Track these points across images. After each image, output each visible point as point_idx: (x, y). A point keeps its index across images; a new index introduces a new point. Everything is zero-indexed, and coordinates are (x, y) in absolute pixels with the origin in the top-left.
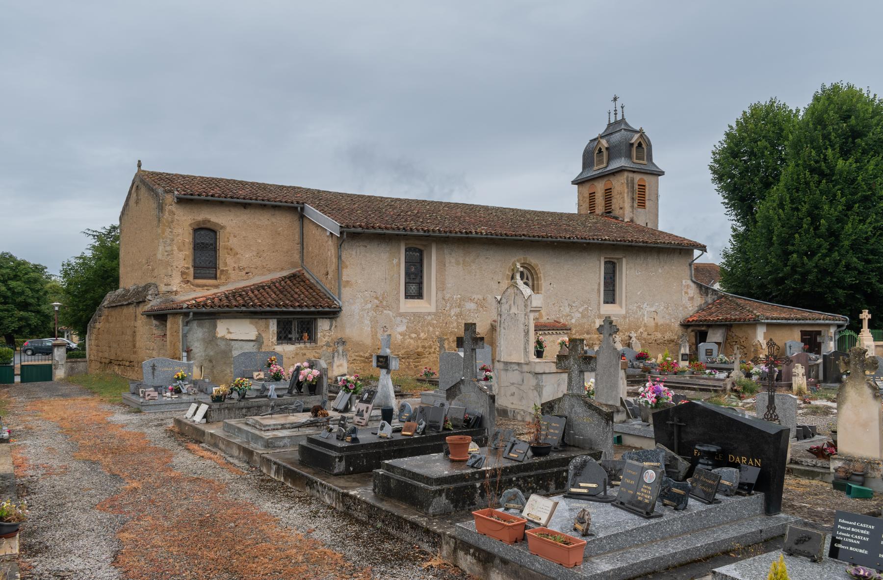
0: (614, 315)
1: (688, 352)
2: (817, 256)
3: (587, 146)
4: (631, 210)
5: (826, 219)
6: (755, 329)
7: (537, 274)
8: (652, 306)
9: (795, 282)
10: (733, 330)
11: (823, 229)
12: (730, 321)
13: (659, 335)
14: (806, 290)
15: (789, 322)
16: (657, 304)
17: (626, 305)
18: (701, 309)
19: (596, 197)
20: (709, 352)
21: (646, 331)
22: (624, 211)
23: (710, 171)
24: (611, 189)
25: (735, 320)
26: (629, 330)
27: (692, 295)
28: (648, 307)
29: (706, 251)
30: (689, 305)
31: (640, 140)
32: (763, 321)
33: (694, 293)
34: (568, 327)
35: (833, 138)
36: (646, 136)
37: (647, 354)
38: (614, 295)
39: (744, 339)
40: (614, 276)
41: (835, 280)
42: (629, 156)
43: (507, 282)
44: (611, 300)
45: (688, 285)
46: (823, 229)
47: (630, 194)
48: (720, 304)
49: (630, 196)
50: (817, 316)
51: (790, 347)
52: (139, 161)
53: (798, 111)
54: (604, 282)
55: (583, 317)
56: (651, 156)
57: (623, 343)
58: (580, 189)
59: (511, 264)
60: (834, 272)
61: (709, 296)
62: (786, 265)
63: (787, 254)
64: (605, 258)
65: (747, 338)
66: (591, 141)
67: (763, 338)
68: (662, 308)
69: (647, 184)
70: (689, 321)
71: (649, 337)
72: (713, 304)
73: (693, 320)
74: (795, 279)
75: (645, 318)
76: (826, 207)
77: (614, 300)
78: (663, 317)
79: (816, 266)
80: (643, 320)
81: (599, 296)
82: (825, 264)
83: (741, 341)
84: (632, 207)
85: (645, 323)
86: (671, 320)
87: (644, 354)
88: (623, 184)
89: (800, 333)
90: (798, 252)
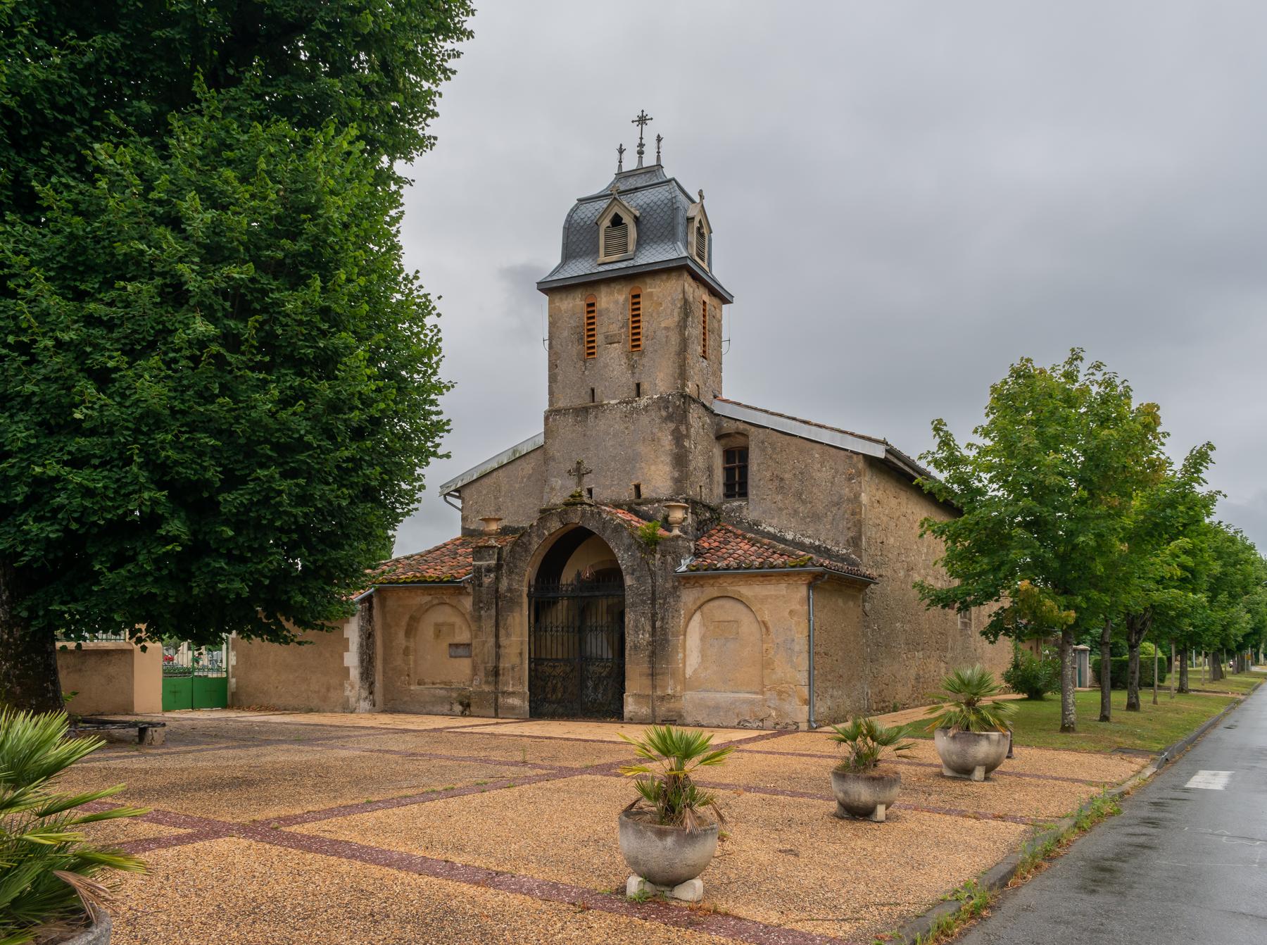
52: (659, 136)
53: (395, 530)
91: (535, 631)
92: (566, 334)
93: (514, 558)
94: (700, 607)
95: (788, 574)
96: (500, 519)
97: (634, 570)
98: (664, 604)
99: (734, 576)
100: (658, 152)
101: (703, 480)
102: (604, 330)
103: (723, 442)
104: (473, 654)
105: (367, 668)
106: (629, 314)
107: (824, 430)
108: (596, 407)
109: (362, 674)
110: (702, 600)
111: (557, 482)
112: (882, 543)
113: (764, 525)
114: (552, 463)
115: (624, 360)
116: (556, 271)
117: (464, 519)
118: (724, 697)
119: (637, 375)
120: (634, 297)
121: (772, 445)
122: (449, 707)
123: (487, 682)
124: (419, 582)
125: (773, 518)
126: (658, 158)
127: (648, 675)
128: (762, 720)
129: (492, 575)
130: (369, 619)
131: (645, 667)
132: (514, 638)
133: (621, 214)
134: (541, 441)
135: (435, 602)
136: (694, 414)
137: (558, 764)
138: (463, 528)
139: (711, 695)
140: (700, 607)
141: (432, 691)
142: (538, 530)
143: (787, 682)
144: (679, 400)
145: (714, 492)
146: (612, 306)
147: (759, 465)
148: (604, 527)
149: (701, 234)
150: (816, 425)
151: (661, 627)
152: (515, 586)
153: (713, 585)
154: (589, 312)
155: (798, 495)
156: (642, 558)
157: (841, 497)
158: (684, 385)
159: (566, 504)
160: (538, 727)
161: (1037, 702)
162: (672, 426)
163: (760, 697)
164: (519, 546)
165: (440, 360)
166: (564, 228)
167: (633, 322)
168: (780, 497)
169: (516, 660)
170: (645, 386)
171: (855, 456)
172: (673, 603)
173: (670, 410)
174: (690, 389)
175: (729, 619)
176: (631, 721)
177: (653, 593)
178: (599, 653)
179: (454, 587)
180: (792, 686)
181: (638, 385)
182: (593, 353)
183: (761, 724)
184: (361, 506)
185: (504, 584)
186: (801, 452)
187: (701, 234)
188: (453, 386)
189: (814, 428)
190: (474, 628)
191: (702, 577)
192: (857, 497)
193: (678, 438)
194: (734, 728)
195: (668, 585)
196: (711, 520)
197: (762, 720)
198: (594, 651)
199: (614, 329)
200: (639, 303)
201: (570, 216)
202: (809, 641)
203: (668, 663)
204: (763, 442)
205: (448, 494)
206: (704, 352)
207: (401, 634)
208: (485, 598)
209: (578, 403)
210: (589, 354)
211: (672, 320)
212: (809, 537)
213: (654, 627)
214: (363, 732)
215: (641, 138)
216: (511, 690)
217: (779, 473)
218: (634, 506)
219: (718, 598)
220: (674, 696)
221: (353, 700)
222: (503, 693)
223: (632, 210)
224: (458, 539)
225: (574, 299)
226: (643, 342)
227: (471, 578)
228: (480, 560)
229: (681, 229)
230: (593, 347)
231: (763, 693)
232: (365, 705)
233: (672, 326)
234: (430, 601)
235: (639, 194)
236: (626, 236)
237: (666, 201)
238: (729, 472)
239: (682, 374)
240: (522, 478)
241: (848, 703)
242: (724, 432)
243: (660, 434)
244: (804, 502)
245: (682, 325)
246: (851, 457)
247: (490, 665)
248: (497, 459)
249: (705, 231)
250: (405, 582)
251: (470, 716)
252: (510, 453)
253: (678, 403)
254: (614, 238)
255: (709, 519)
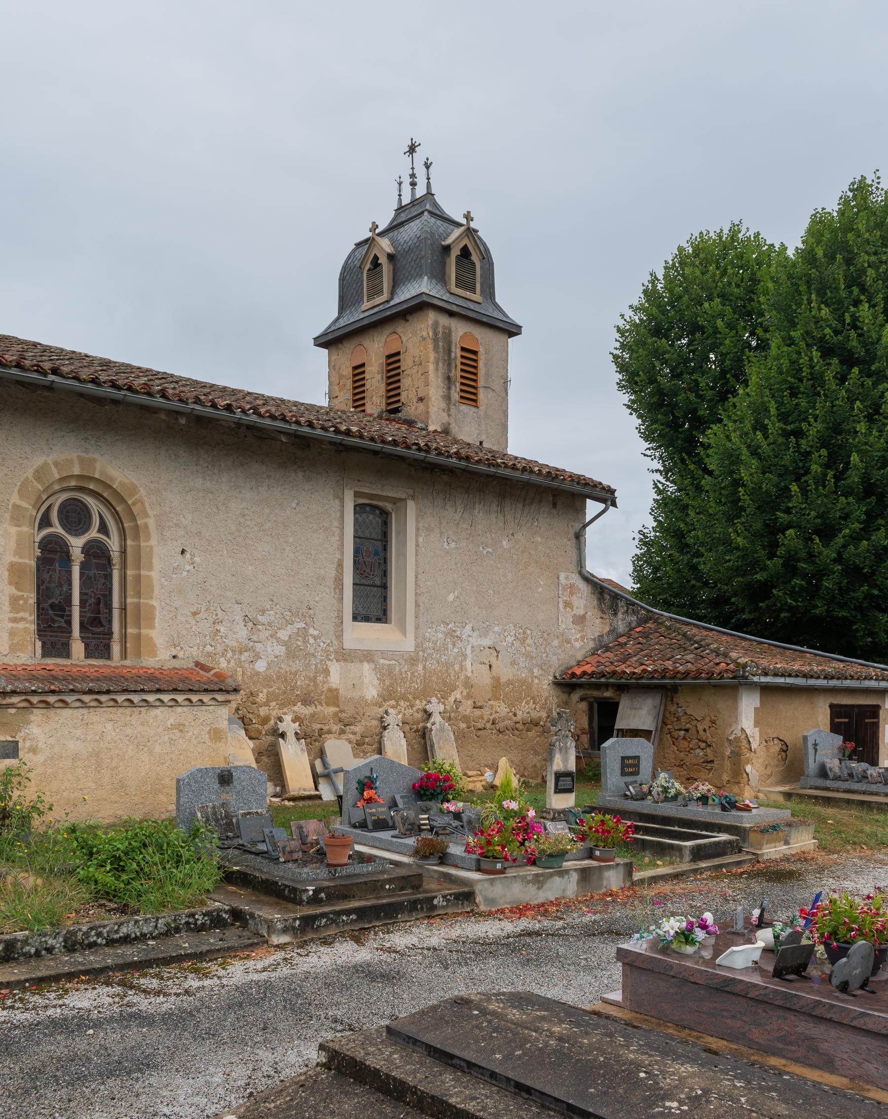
0: (382, 652)
1: (572, 766)
2: (840, 535)
3: (349, 257)
4: (443, 405)
5: (862, 453)
6: (735, 699)
7: (133, 518)
8: (484, 634)
9: (793, 594)
10: (680, 699)
11: (854, 478)
12: (674, 678)
13: (503, 709)
14: (817, 611)
15: (811, 682)
16: (496, 629)
17: (417, 628)
18: (602, 646)
19: (367, 376)
20: (631, 766)
21: (469, 696)
22: (427, 407)
23: (614, 367)
24: (398, 353)
25: (687, 674)
26: (425, 693)
27: (581, 612)
28: (476, 634)
29: (614, 504)
30: (574, 634)
31: (466, 241)
32: (756, 679)
33: (586, 606)
34: (230, 683)
35: (869, 281)
36: (480, 238)
37: (447, 778)
38: (385, 599)
39: (706, 724)
40: (385, 548)
41: (876, 592)
42: (440, 277)
43: (13, 530)
44: (380, 613)
45: (572, 586)
46: (854, 478)
47: (441, 365)
48: (646, 635)
49: (441, 370)
50: (864, 671)
51: (815, 745)
54: (355, 562)
55: (291, 654)
56: (491, 286)
57: (407, 728)
58: (334, 357)
59: (30, 473)
60: (873, 573)
61: (620, 615)
62: (771, 556)
63: (773, 531)
64: (357, 494)
65: (713, 722)
66: (359, 245)
67: (752, 723)
68: (510, 639)
69: (481, 350)
70: (573, 675)
71: (478, 712)
72: (628, 635)
73: (584, 673)
74: (794, 587)
75: (468, 664)
76: (862, 427)
77: (385, 612)
78: (513, 663)
79: (839, 559)
80: (462, 668)
81: (341, 600)
82: (858, 555)
83: (700, 728)
84: (448, 398)
85: (467, 677)
86: (531, 671)
87: (437, 779)
88: (424, 339)
89: (828, 711)
90: (798, 527)
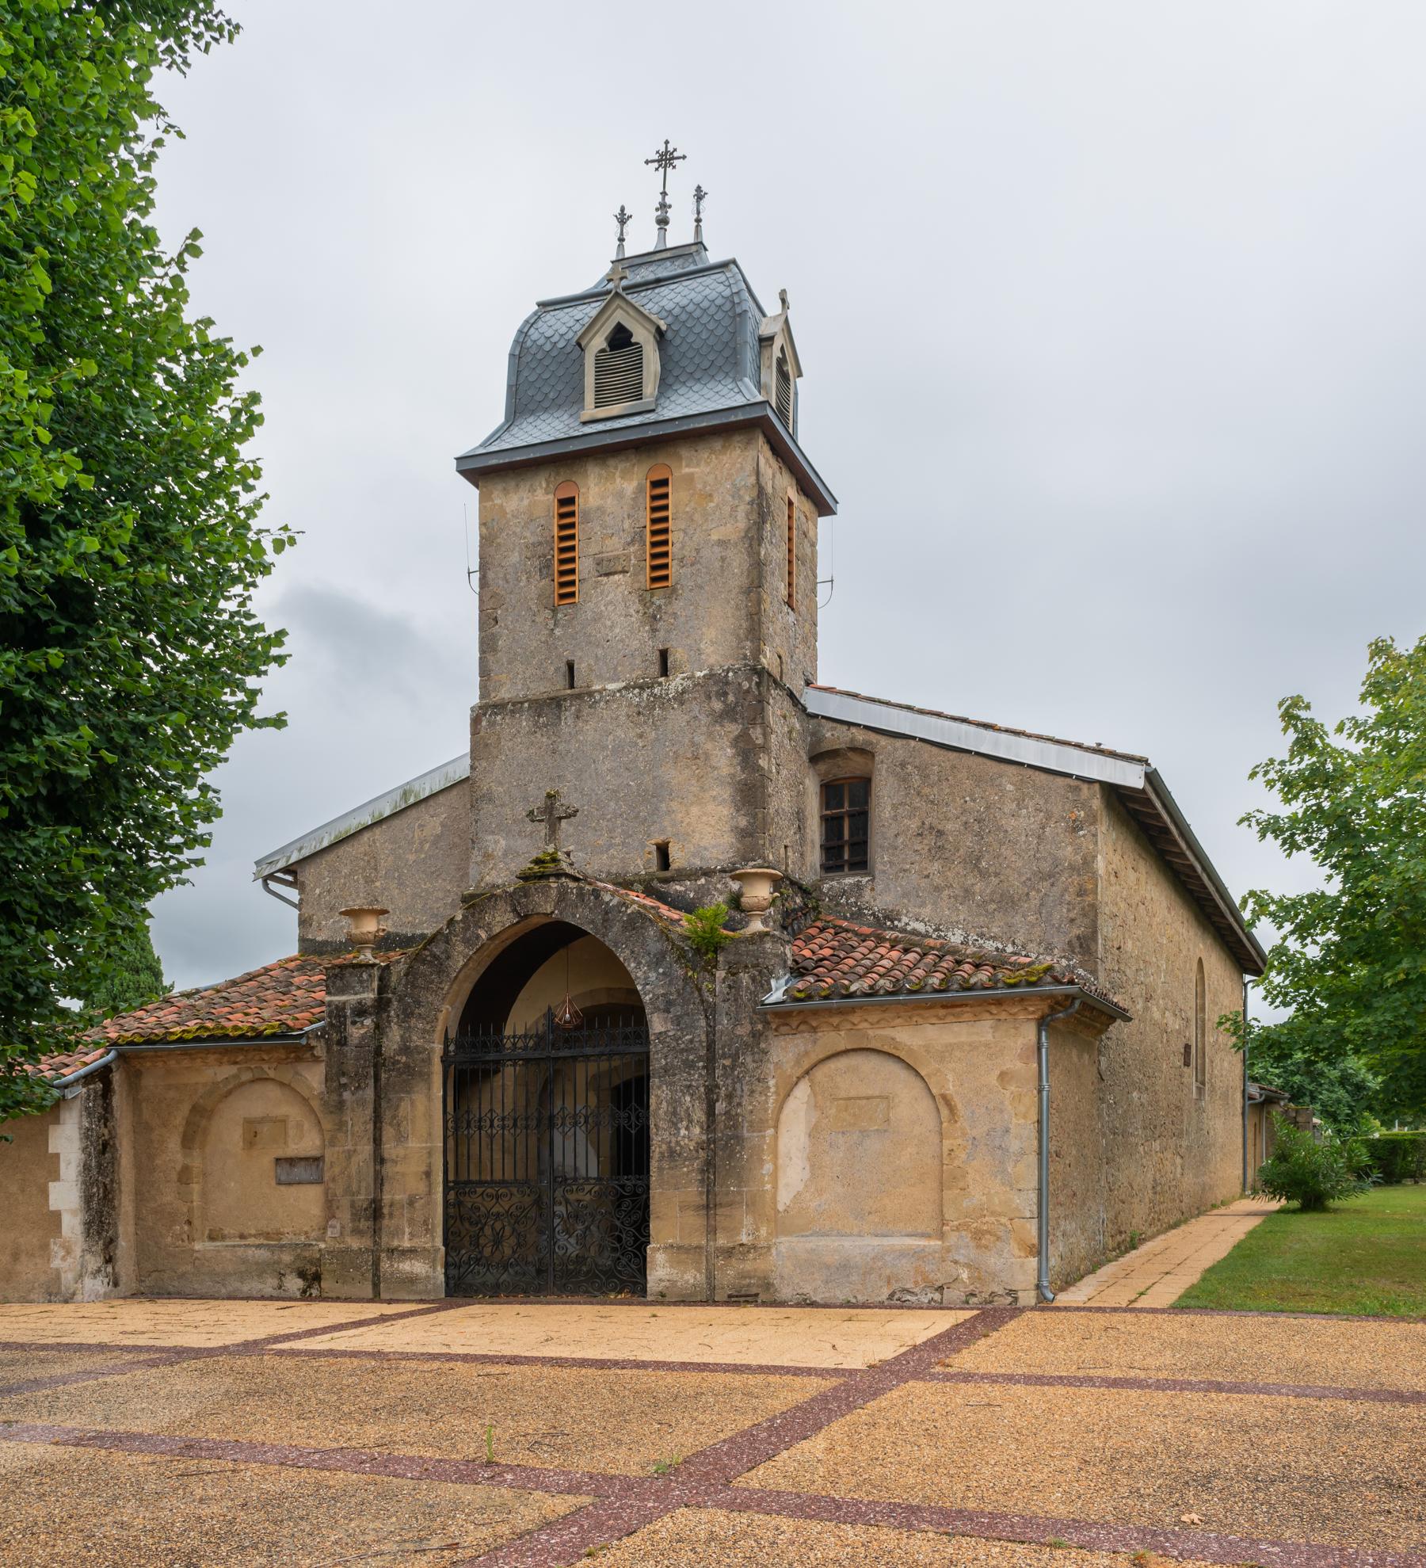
52: (699, 188)
91: (456, 1129)
92: (515, 557)
93: (414, 986)
94: (807, 1072)
95: (999, 1002)
96: (384, 912)
97: (669, 1004)
98: (733, 1068)
99: (884, 1007)
100: (698, 221)
101: (790, 836)
102: (593, 549)
103: (822, 767)
104: (326, 1179)
105: (100, 1213)
106: (645, 517)
107: (1023, 740)
108: (579, 696)
109: (88, 1225)
110: (814, 1058)
111: (497, 843)
112: (1119, 948)
113: (905, 919)
114: (487, 808)
115: (635, 607)
116: (496, 436)
117: (303, 922)
118: (860, 1246)
119: (661, 634)
120: (655, 484)
121: (923, 770)
122: (275, 1282)
123: (356, 1231)
124: (212, 1038)
125: (923, 905)
126: (698, 229)
127: (698, 1208)
128: (940, 1289)
129: (368, 1022)
130: (105, 1115)
131: (693, 1192)
132: (413, 1144)
133: (630, 325)
134: (463, 771)
135: (246, 1076)
136: (776, 708)
137: (581, 1465)
138: (302, 940)
139: (832, 1243)
140: (807, 1072)
141: (240, 1252)
142: (466, 929)
143: (993, 1213)
144: (750, 680)
145: (808, 862)
146: (610, 503)
147: (895, 807)
148: (605, 921)
149: (784, 376)
150: (1007, 731)
151: (727, 1113)
152: (417, 1041)
153: (837, 1028)
154: (562, 516)
155: (973, 862)
156: (686, 979)
157: (1056, 862)
158: (757, 652)
159: (525, 877)
160: (474, 1327)
161: (1316, 1216)
162: (734, 729)
163: (935, 1243)
164: (424, 962)
165: (258, 504)
166: (512, 355)
167: (654, 533)
168: (936, 865)
169: (418, 1187)
170: (677, 655)
171: (1085, 787)
172: (751, 1066)
173: (731, 698)
174: (768, 660)
175: (870, 1093)
176: (663, 1299)
177: (711, 1046)
178: (569, 1161)
179: (284, 1046)
180: (1003, 1220)
181: (664, 655)
182: (572, 594)
183: (937, 1296)
184: (44, 832)
185: (393, 1038)
186: (979, 780)
187: (784, 376)
188: (292, 541)
189: (1004, 736)
190: (327, 1125)
191: (815, 1012)
192: (1088, 862)
193: (747, 752)
194: (881, 1306)
195: (740, 1031)
196: (804, 910)
197: (940, 1289)
198: (569, 1161)
199: (614, 546)
200: (665, 496)
201: (523, 334)
202: (1040, 1132)
203: (740, 1182)
204: (903, 765)
205: (271, 877)
206: (790, 596)
207: (174, 1143)
208: (350, 1066)
209: (540, 689)
210: (562, 596)
211: (735, 526)
212: (994, 938)
213: (710, 1112)
214: (78, 1363)
215: (664, 194)
216: (407, 1244)
217: (935, 822)
218: (656, 884)
219: (846, 1052)
220: (755, 1247)
221: (68, 1278)
222: (391, 1251)
223: (653, 317)
224: (292, 960)
225: (532, 490)
226: (673, 571)
227: (323, 1028)
228: (342, 992)
229: (749, 355)
230: (572, 583)
231: (941, 1236)
232: (96, 1285)
233: (734, 537)
234: (235, 1076)
235: (664, 291)
236: (639, 367)
237: (719, 302)
238: (831, 824)
239: (754, 629)
240: (421, 844)
241: (1083, 1244)
242: (826, 747)
243: (709, 746)
244: (984, 874)
245: (754, 537)
246: (1077, 789)
247: (363, 1197)
248: (370, 809)
249: (790, 368)
250: (180, 1040)
251: (322, 1298)
252: (397, 796)
253: (746, 685)
254: (615, 371)
255: (801, 909)
